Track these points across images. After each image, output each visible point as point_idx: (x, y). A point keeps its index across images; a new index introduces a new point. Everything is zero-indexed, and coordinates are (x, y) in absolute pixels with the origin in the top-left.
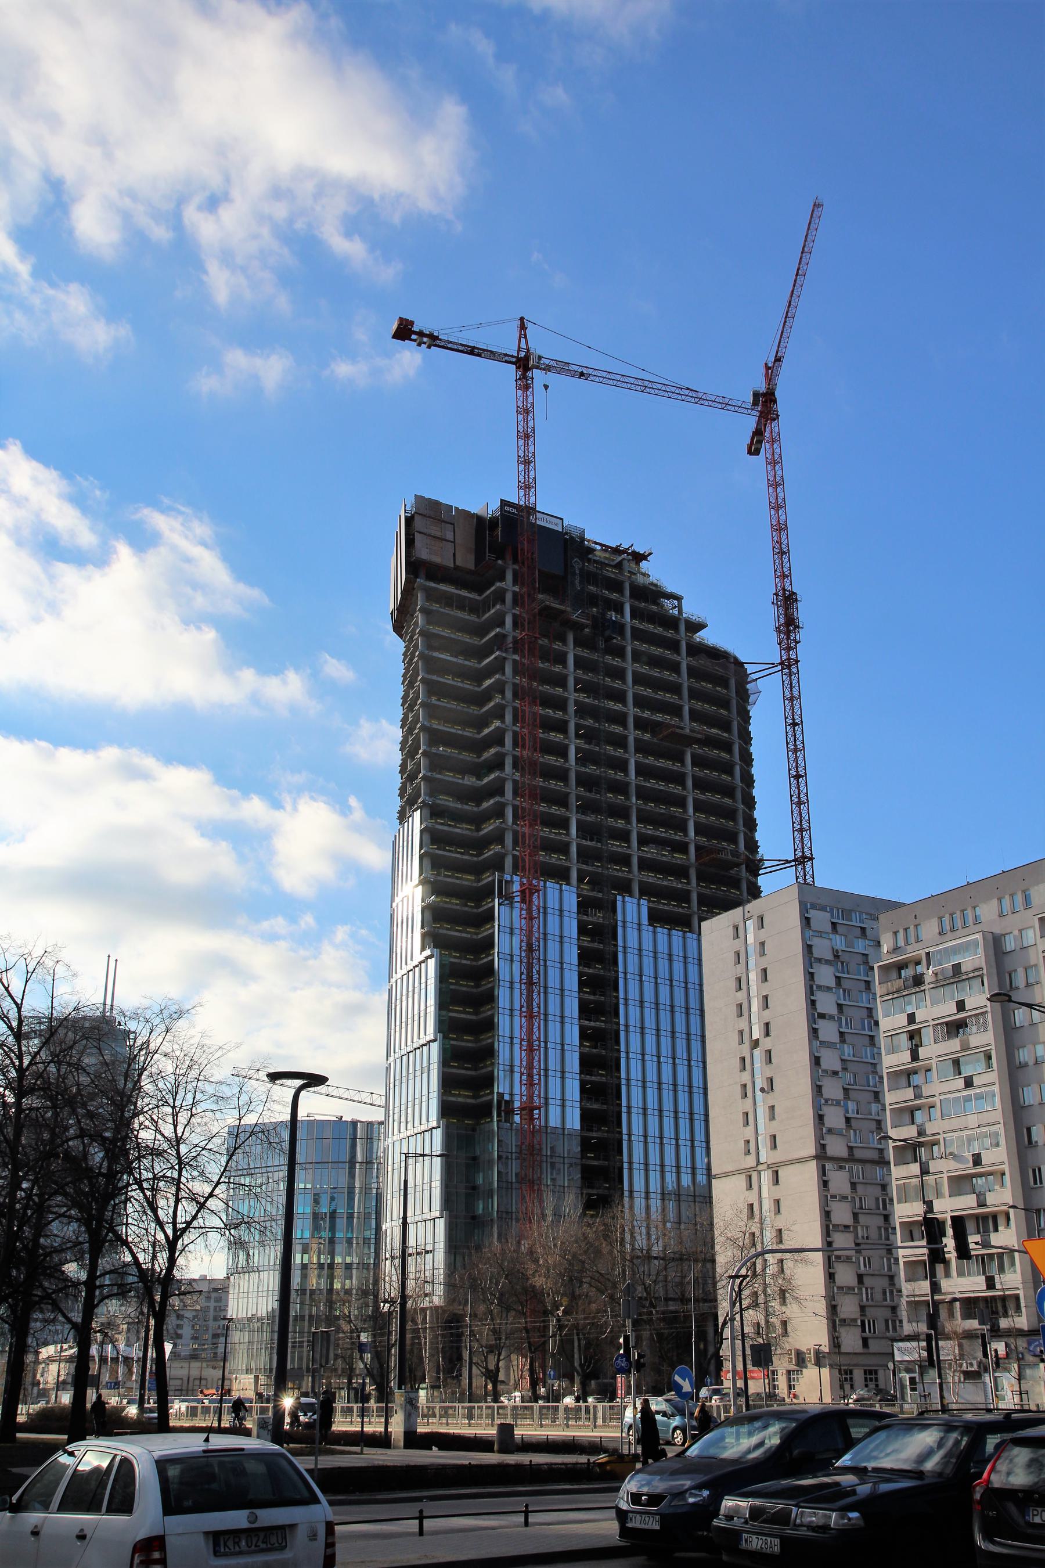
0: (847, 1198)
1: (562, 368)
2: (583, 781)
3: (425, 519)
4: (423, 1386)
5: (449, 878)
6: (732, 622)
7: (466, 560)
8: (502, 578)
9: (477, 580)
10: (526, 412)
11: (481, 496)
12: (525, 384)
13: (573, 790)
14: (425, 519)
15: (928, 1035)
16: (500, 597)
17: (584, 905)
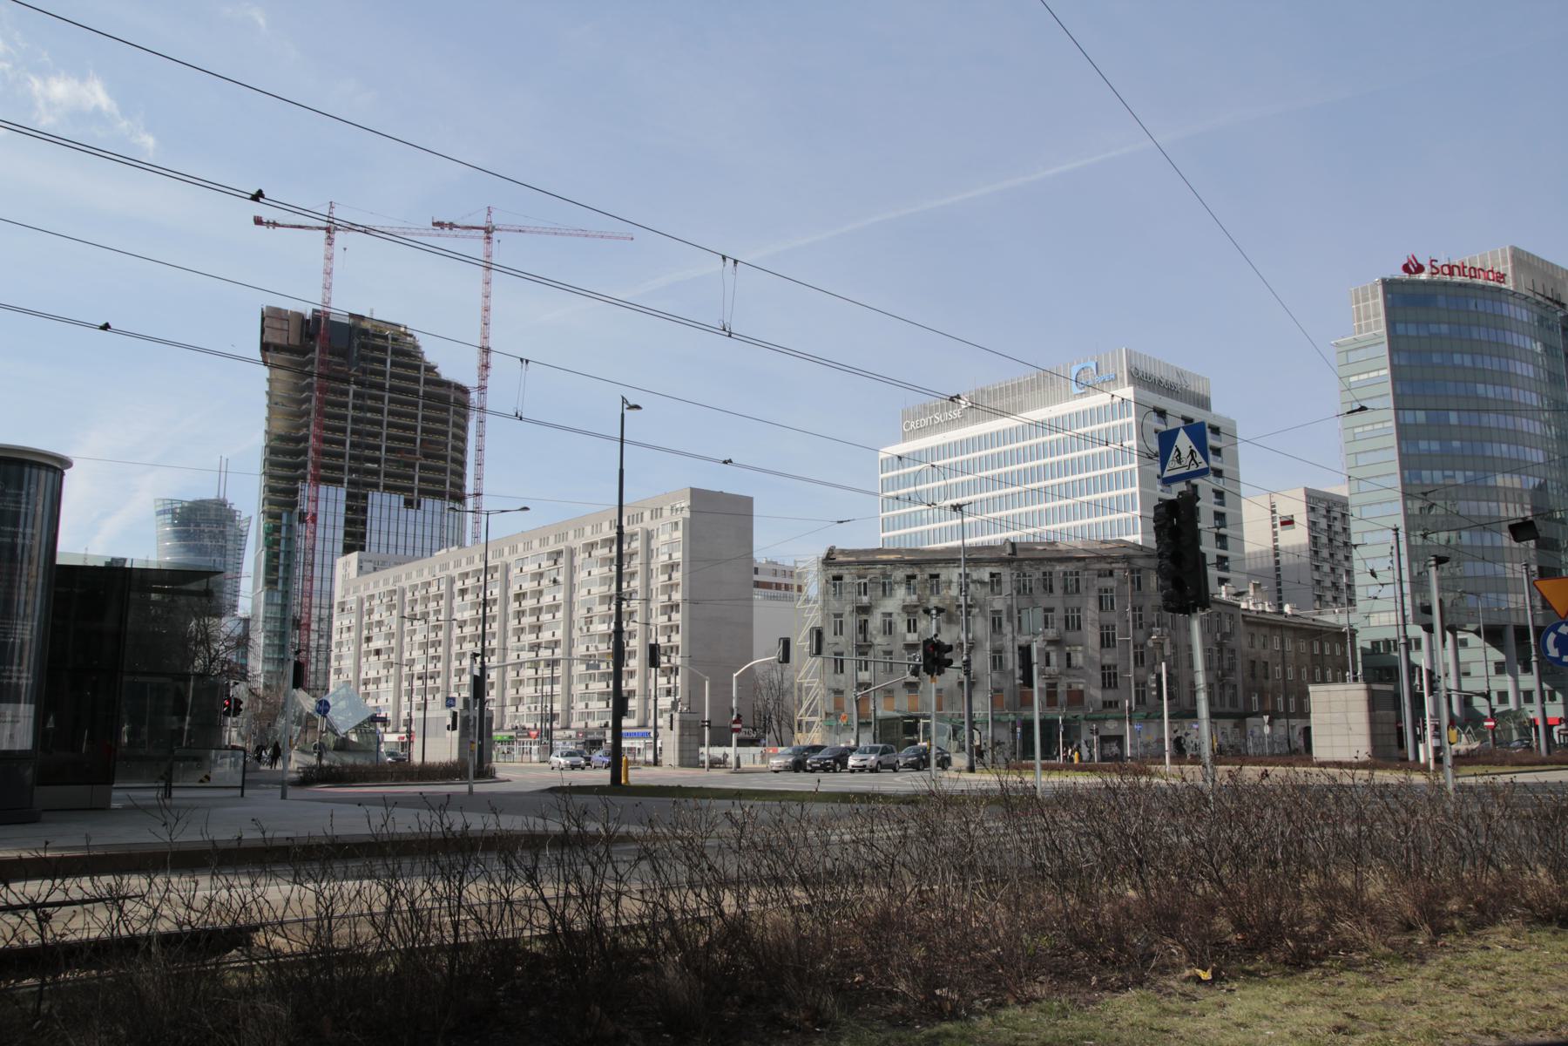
0: (1283, 524)
1: (352, 227)
2: (352, 457)
3: (271, 318)
4: (1200, 613)
5: (274, 483)
6: (451, 361)
7: (294, 340)
8: (314, 351)
9: (301, 350)
10: (329, 258)
11: (303, 301)
12: (330, 241)
13: (347, 463)
14: (271, 318)
15: (596, 620)
16: (311, 362)
17: (350, 496)
